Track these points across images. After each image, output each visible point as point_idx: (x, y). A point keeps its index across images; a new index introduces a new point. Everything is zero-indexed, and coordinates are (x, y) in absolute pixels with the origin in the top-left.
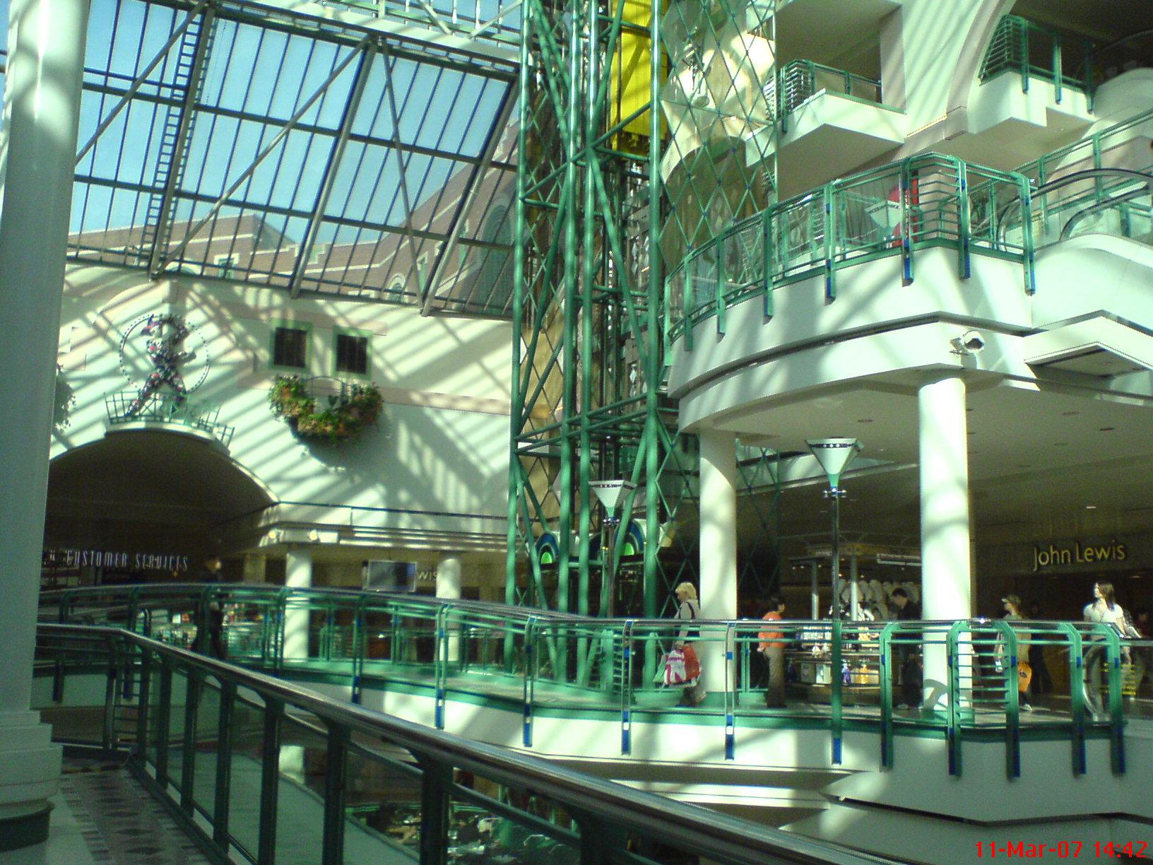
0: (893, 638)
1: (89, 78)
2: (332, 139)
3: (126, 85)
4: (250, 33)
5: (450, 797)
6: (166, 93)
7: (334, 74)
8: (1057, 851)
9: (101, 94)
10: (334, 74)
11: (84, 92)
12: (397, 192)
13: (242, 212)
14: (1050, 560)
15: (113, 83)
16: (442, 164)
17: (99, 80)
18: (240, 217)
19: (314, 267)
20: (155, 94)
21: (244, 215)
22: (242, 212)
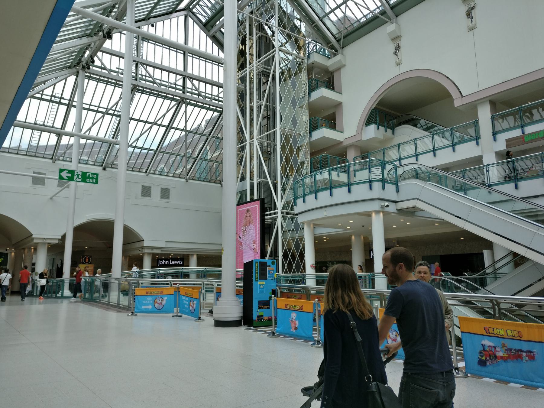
0: (277, 212)
1: (84, 106)
2: (66, 107)
3: (104, 110)
4: (145, 97)
5: (136, 263)
6: (116, 113)
7: (168, 111)
8: (416, 162)
9: (39, 101)
10: (168, 111)
11: (83, 110)
12: (189, 146)
13: (86, 141)
14: (82, 260)
15: (100, 109)
16: (141, 124)
17: (87, 107)
18: (86, 142)
19: (132, 160)
20: (96, 109)
21: (87, 142)
22: (86, 141)
